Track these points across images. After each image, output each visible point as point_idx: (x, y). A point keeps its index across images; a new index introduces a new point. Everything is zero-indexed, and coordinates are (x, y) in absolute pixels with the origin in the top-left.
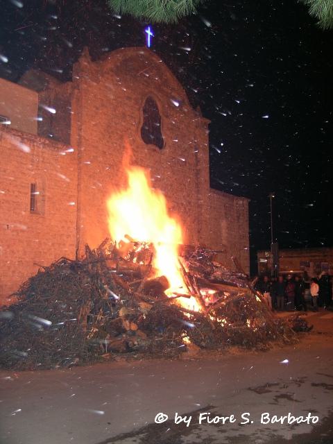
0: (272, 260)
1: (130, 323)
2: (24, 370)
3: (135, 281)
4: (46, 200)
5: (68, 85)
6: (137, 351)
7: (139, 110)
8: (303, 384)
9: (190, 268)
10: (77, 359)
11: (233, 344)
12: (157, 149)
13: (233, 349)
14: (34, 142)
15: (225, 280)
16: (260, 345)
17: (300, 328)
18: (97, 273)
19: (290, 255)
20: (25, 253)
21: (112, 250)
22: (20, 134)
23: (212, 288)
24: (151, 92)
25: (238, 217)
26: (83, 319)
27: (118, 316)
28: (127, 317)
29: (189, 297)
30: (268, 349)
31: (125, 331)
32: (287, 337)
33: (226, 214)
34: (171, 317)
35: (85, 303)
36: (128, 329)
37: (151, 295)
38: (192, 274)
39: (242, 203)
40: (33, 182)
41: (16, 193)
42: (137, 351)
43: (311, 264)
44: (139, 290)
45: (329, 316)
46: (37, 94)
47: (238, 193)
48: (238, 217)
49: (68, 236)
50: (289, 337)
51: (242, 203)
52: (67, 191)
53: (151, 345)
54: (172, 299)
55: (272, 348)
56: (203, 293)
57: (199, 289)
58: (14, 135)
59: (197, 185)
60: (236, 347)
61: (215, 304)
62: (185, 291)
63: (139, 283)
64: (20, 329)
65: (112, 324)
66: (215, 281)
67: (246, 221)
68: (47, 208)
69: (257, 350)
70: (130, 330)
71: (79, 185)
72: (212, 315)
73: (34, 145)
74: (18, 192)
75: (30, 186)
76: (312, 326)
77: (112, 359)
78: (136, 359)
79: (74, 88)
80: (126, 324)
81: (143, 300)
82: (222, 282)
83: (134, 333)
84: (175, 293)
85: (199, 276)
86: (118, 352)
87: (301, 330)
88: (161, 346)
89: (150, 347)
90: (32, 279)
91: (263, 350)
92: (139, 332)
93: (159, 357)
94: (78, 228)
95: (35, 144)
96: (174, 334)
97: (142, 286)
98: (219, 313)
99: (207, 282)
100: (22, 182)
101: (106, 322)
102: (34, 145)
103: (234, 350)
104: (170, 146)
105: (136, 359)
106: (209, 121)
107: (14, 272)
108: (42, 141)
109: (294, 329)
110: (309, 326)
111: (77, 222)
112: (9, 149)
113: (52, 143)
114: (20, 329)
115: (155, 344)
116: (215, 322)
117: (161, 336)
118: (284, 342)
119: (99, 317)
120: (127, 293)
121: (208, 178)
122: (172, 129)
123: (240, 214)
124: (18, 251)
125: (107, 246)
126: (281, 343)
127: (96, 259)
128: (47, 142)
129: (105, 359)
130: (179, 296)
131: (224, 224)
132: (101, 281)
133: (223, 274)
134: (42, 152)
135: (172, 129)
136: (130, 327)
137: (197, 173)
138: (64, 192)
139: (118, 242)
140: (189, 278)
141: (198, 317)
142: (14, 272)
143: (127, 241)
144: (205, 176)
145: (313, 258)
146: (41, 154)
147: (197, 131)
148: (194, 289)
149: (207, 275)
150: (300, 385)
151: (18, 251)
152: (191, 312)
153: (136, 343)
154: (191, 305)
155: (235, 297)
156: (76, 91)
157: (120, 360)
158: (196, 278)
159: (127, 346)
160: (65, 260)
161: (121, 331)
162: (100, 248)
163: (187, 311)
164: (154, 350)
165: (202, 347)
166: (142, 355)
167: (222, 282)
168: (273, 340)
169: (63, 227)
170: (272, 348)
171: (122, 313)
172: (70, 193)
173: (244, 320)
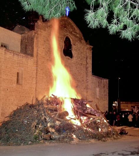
0: (117, 105)
1: (52, 129)
2: (9, 145)
3: (55, 112)
4: (23, 79)
5: (33, 32)
6: (54, 139)
7: (62, 42)
8: (114, 154)
9: (77, 108)
10: (30, 142)
11: (93, 138)
12: (70, 58)
13: (92, 140)
14: (18, 55)
15: (92, 113)
16: (104, 139)
17: (122, 133)
18: (40, 109)
19: (127, 103)
20: (14, 100)
21: (46, 100)
22: (13, 52)
23: (85, 116)
24: (68, 35)
25: (104, 87)
26: (33, 127)
27: (47, 126)
28: (51, 126)
29: (75, 120)
30: (106, 141)
31: (49, 132)
32: (116, 136)
33: (99, 85)
34: (68, 128)
35: (34, 121)
36: (51, 131)
37: (61, 118)
38: (78, 111)
39: (106, 81)
40: (18, 72)
41: (11, 76)
42: (54, 139)
43: (136, 107)
44: (56, 116)
45: (137, 129)
46: (20, 35)
47: (105, 77)
48: (104, 87)
49: (32, 94)
50: (117, 136)
51: (106, 81)
52: (32, 75)
53: (60, 137)
54: (69, 120)
55: (108, 140)
56: (82, 118)
57: (80, 116)
58: (10, 52)
59: (87, 74)
60: (94, 139)
61: (87, 122)
62: (74, 117)
63: (57, 113)
64: (10, 130)
65: (45, 129)
66: (87, 113)
67: (107, 88)
68: (23, 82)
69: (102, 141)
70: (52, 132)
71: (37, 73)
72: (85, 127)
73: (18, 57)
74: (12, 76)
75: (17, 73)
76: (128, 133)
77: (44, 143)
78: (53, 143)
79: (35, 33)
80: (50, 129)
81: (58, 120)
82: (90, 114)
83: (53, 133)
84: (70, 118)
85: (81, 111)
86: (47, 140)
87: (123, 134)
88: (63, 138)
89: (59, 138)
90: (15, 111)
91: (104, 141)
92: (55, 133)
93: (62, 142)
94: (36, 90)
95: (19, 56)
96: (69, 134)
97: (57, 115)
98: (88, 126)
99: (84, 113)
100: (13, 72)
101: (43, 128)
102: (18, 57)
103: (93, 141)
104: (75, 57)
105: (53, 143)
106: (92, 47)
107: (10, 108)
108: (22, 55)
109: (120, 133)
110: (126, 132)
111: (36, 88)
112: (8, 58)
113: (26, 56)
114: (10, 130)
115: (61, 137)
116: (86, 130)
117: (64, 134)
118: (114, 138)
119: (40, 126)
120: (51, 117)
121: (91, 70)
122: (76, 50)
123: (105, 86)
124: (11, 99)
125: (45, 98)
126: (112, 138)
127: (40, 104)
128: (24, 55)
129: (41, 142)
130: (72, 119)
131: (98, 89)
132: (41, 112)
133: (91, 111)
134: (22, 60)
135: (76, 50)
136: (52, 130)
137: (87, 68)
138: (31, 76)
139: (40, 100)
140: (76, 112)
141: (80, 128)
142: (10, 108)
143: (53, 97)
144: (90, 69)
145: (136, 104)
146: (21, 60)
147: (87, 50)
148: (78, 116)
149: (84, 111)
150: (113, 154)
151: (11, 99)
152: (76, 126)
153: (54, 137)
154: (77, 123)
155: (94, 120)
156: (36, 34)
157: (47, 143)
158: (80, 112)
159: (50, 138)
160: (27, 104)
161: (47, 132)
162: (41, 100)
163: (74, 125)
164: (60, 140)
165: (80, 139)
166: (56, 141)
167: (90, 114)
168: (109, 137)
169: (30, 90)
170: (108, 140)
171: (49, 125)
172: (33, 76)
173: (98, 128)
